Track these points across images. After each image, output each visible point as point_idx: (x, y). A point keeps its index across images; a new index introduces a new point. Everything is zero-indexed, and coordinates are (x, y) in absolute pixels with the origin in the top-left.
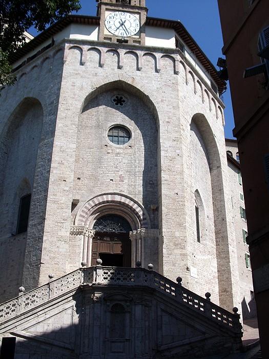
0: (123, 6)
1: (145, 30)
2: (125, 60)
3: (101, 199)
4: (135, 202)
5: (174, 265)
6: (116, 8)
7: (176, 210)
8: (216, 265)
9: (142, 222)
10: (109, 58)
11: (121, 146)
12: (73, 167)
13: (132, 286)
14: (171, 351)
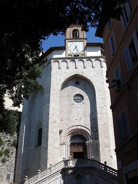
0: (76, 39)
1: (86, 49)
2: (78, 64)
4: (87, 128)
6: (73, 40)
7: (105, 131)
10: (71, 64)
11: (80, 104)
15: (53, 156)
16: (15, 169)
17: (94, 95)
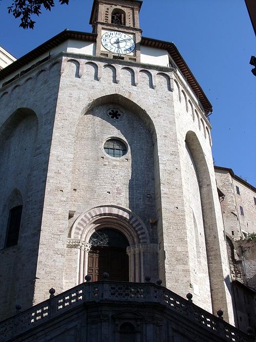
2: (121, 76)
5: (177, 281)
6: (111, 28)
10: (105, 73)
11: (118, 159)
12: (71, 177)
13: (143, 303)
15: (50, 272)
17: (150, 145)
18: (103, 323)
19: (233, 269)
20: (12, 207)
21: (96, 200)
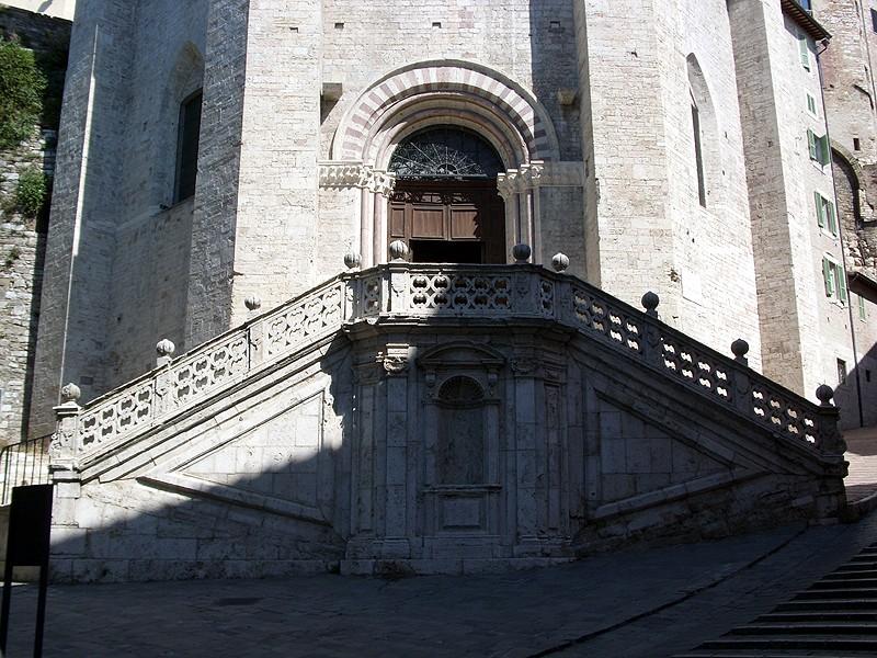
3: (406, 81)
4: (511, 85)
8: (753, 276)
9: (533, 145)
13: (504, 321)
14: (628, 522)
15: (272, 256)
16: (31, 361)
18: (390, 381)
19: (854, 244)
20: (186, 94)
21: (400, 48)
